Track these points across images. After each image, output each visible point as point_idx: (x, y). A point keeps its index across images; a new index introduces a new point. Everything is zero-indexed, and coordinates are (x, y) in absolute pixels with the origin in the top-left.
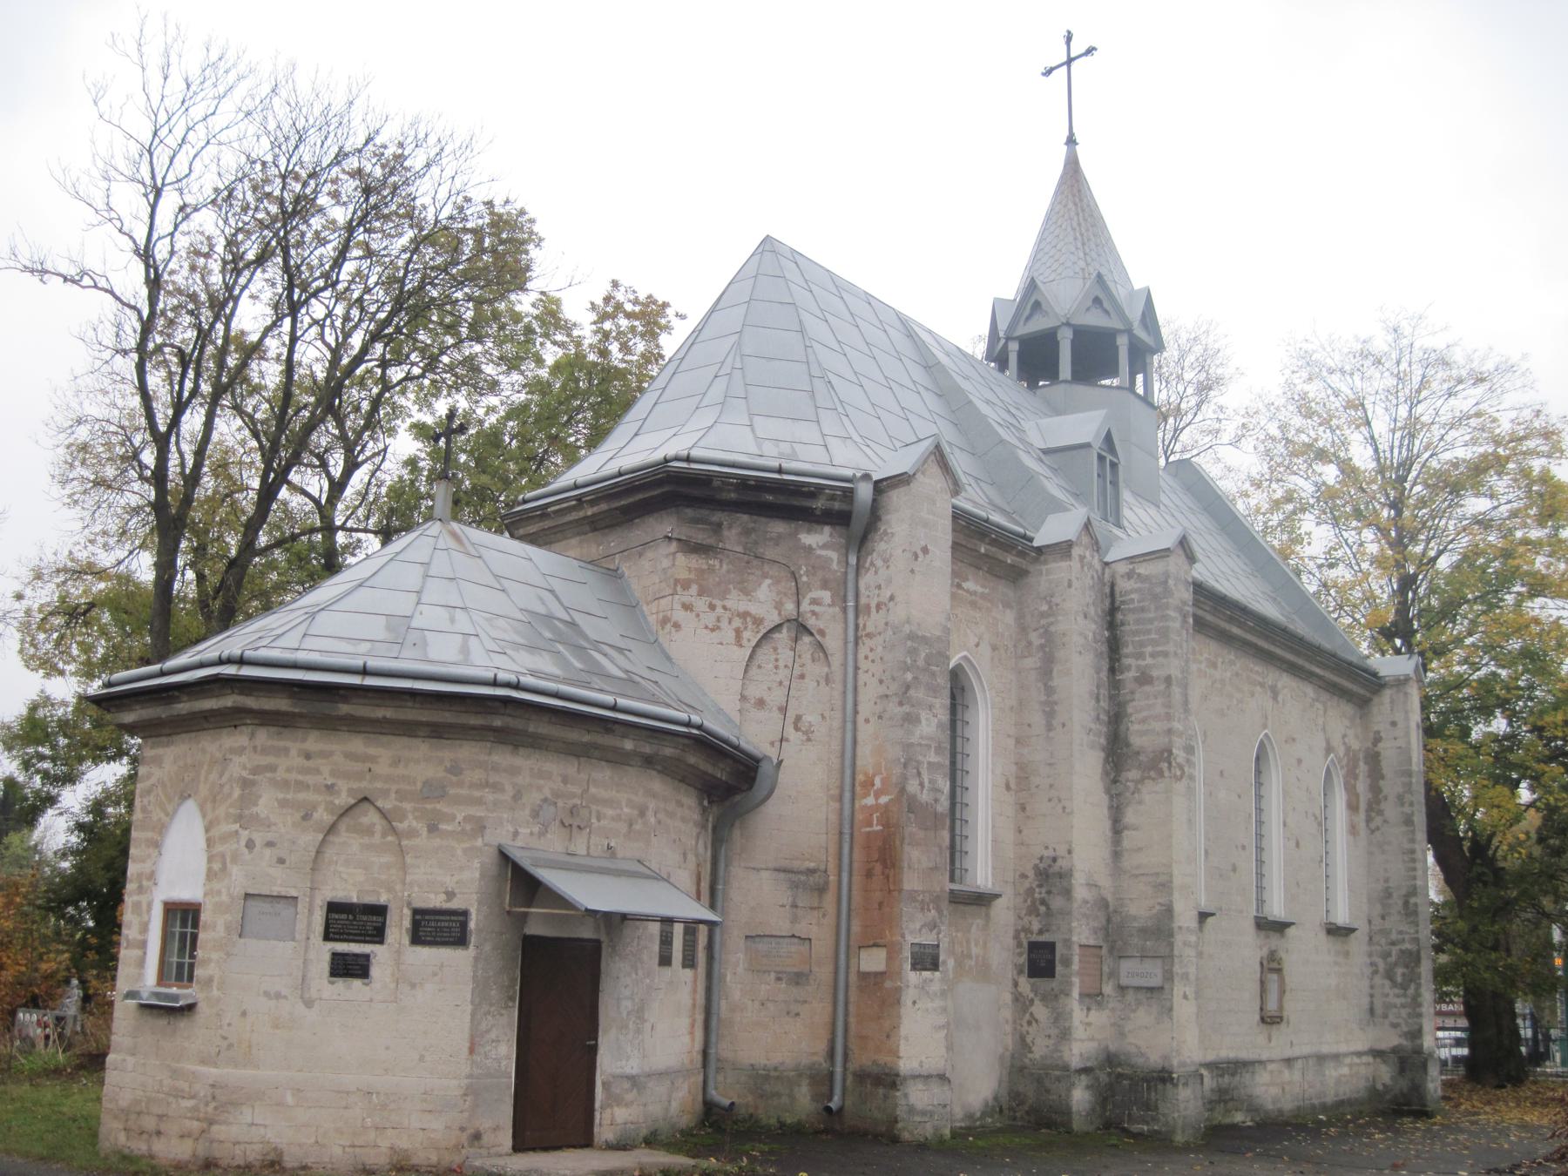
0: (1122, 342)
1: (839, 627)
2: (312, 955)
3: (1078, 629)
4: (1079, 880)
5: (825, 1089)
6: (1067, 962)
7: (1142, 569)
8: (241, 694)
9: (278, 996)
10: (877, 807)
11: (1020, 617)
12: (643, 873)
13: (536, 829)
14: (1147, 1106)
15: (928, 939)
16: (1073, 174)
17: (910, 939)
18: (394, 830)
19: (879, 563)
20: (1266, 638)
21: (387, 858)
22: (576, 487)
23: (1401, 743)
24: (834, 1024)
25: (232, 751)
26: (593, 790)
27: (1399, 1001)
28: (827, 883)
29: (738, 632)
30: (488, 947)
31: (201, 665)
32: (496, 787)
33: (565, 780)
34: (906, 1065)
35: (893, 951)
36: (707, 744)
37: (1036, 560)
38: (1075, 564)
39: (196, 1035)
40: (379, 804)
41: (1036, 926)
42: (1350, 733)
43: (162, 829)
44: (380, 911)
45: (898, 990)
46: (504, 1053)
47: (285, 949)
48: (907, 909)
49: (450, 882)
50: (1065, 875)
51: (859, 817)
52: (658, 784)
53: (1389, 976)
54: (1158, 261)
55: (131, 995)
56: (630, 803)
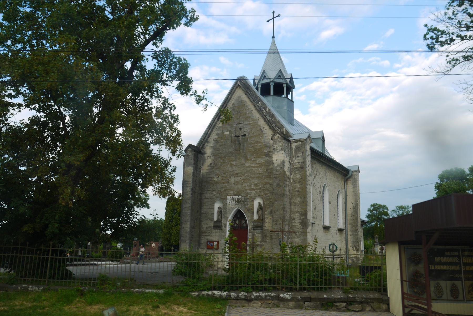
0: (285, 85)
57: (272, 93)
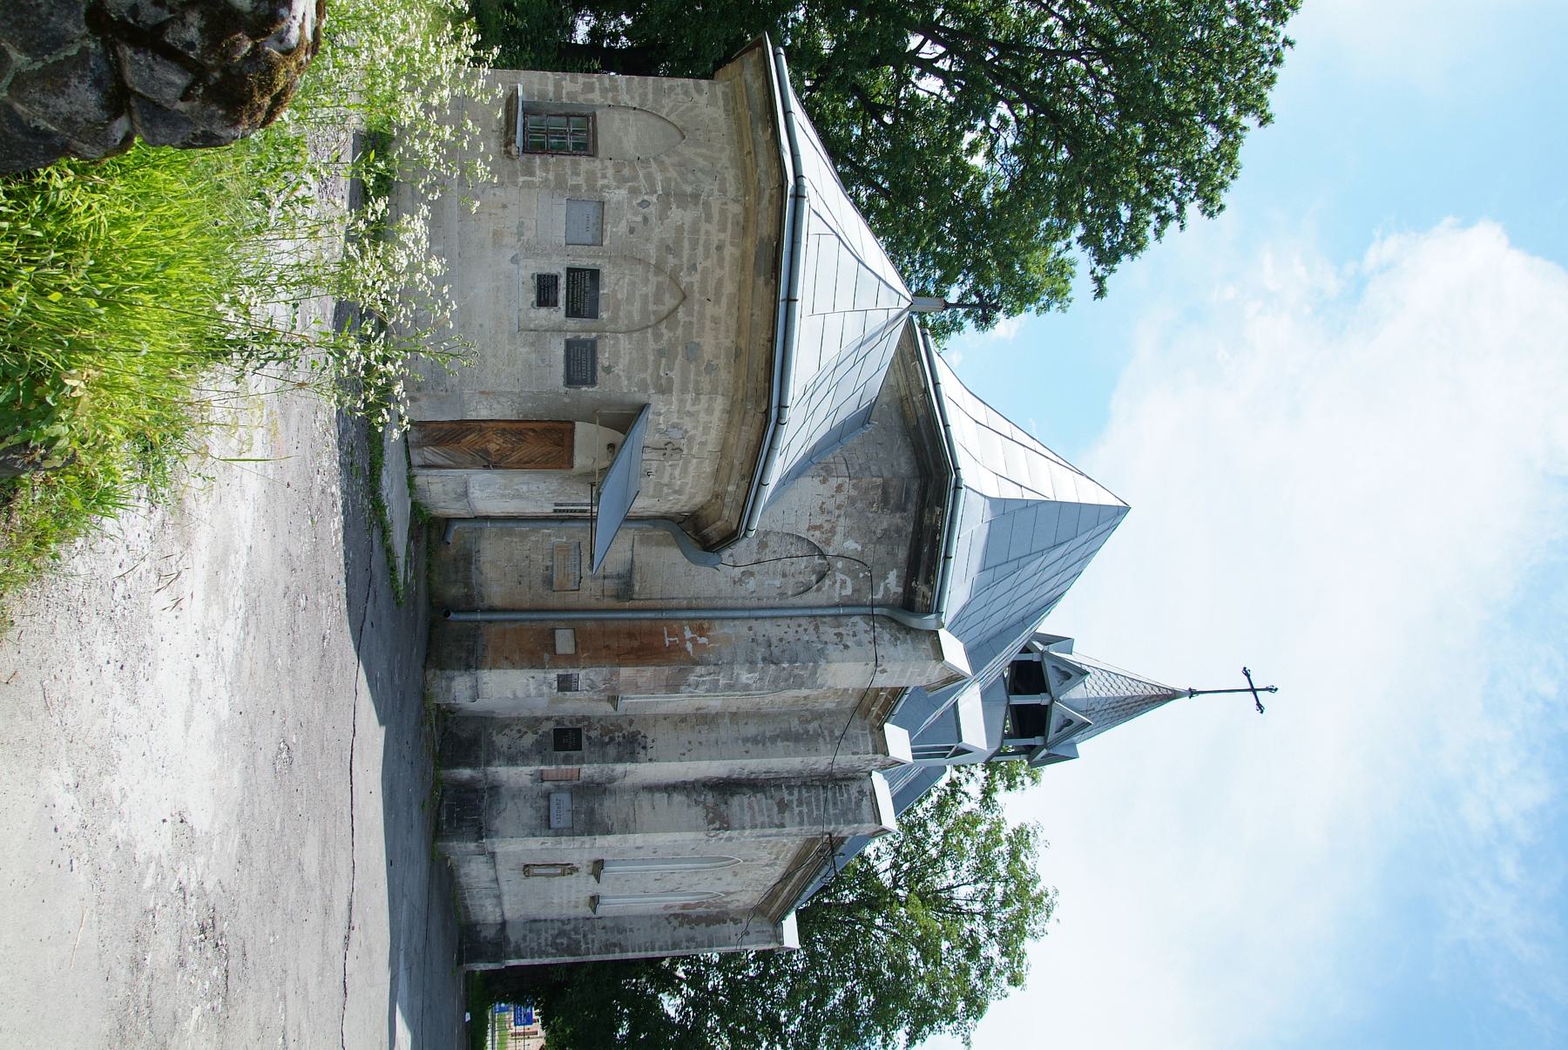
0: (1038, 741)
4: (629, 766)
6: (567, 761)
7: (866, 803)
9: (520, 234)
10: (684, 641)
14: (460, 820)
15: (583, 683)
16: (1173, 695)
18: (659, 322)
21: (637, 317)
22: (936, 384)
27: (542, 941)
29: (821, 527)
30: (567, 400)
33: (703, 444)
35: (572, 660)
38: (870, 756)
40: (681, 309)
41: (593, 734)
47: (560, 236)
50: (633, 758)
53: (562, 933)
56: (684, 485)
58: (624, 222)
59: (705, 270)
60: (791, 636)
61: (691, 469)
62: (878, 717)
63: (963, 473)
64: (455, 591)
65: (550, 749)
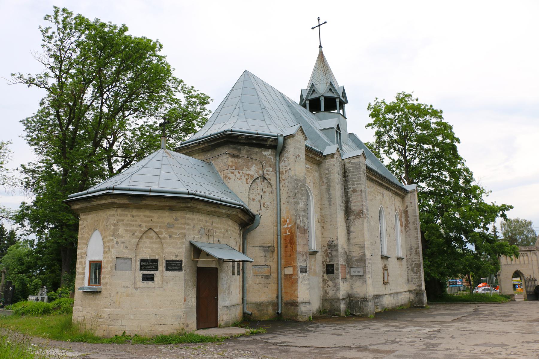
0: (337, 101)
1: (275, 178)
2: (137, 275)
3: (337, 177)
4: (340, 247)
5: (276, 307)
6: (338, 270)
8: (113, 198)
9: (127, 287)
10: (288, 228)
11: (320, 174)
12: (229, 248)
13: (199, 236)
14: (360, 308)
15: (304, 264)
16: (321, 54)
17: (299, 264)
19: (286, 159)
20: (381, 180)
21: (157, 246)
22: (197, 140)
23: (413, 208)
24: (278, 289)
25: (110, 215)
26: (214, 224)
28: (274, 250)
29: (247, 180)
30: (188, 270)
31: (101, 190)
32: (188, 224)
33: (206, 222)
34: (300, 300)
35: (294, 268)
36: (245, 211)
37: (324, 159)
38: (335, 160)
39: (101, 300)
40: (155, 230)
41: (328, 260)
42: (400, 205)
43: (88, 239)
44: (156, 261)
45: (297, 279)
46: (193, 301)
48: (298, 256)
49: (176, 252)
50: (336, 246)
51: (283, 231)
52: (231, 223)
53: (412, 270)
54: (343, 79)
55: (80, 289)
57: (322, 108)
58: (124, 250)
59: (141, 221)
60: (286, 189)
61: (217, 226)
62: (321, 157)
63: (226, 129)
64: (270, 310)
65: (334, 276)
